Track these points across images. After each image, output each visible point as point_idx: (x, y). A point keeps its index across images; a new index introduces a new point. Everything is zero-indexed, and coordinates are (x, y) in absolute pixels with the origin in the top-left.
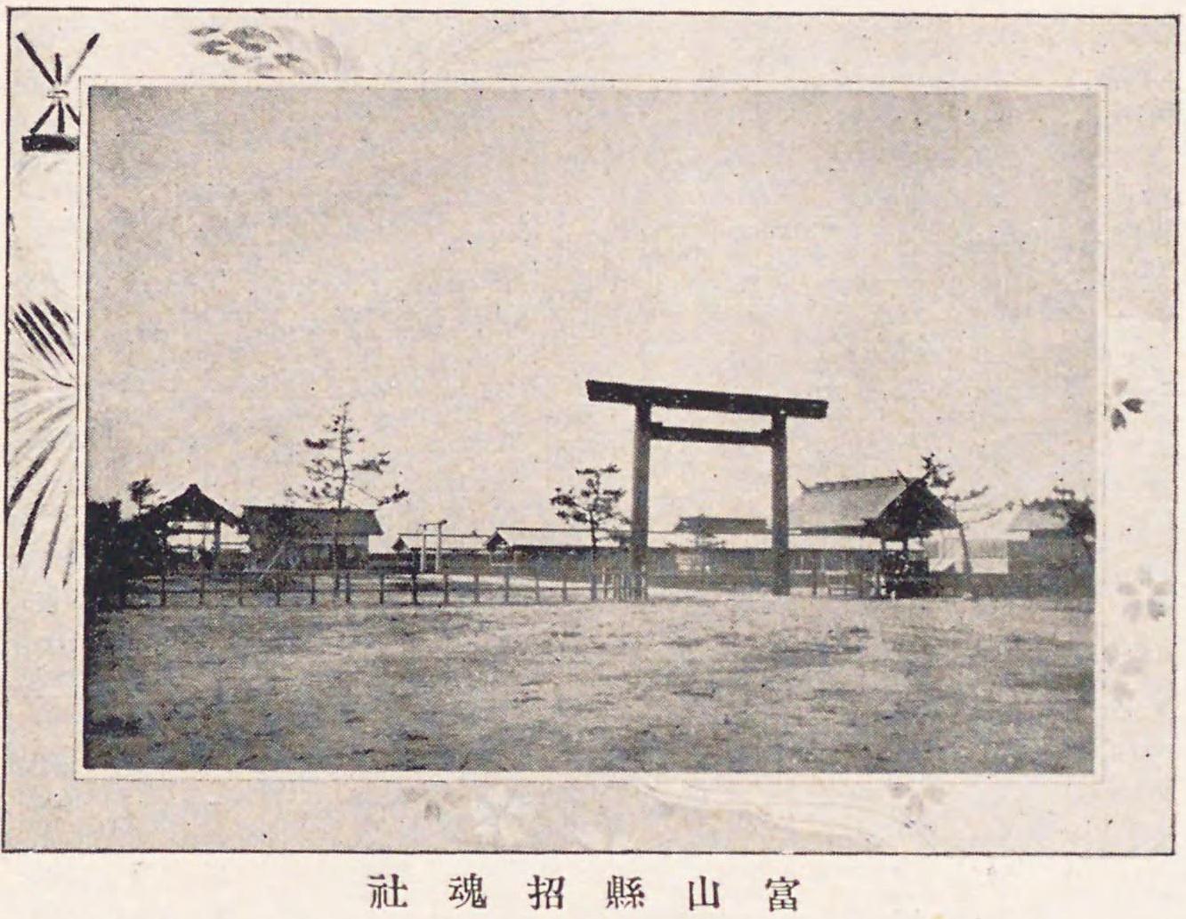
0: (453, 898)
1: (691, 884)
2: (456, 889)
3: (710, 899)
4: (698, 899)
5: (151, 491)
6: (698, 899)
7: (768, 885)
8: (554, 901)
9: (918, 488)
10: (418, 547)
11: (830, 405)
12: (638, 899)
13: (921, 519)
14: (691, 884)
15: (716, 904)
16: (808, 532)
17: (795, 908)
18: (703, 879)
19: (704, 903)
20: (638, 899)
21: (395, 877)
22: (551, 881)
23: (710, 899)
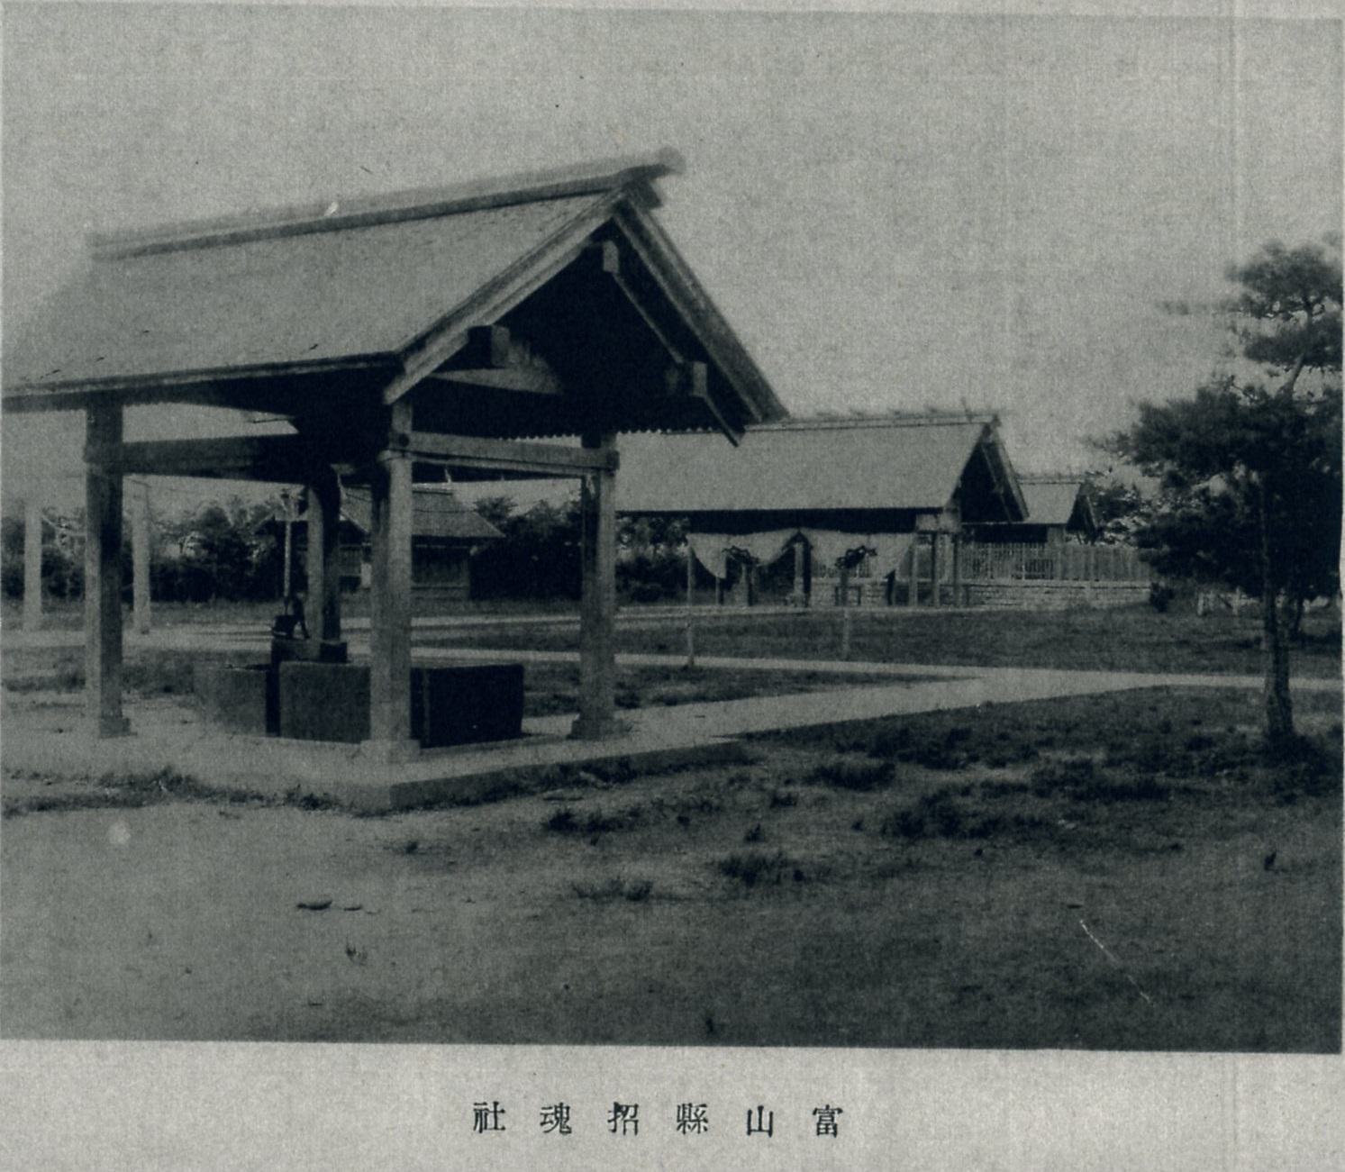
0: (543, 1124)
1: (750, 1113)
2: (546, 1115)
3: (765, 1127)
4: (755, 1126)
5: (272, 498)
6: (755, 1126)
7: (815, 1113)
8: (630, 1126)
9: (1153, 461)
10: (936, 506)
11: (1331, 1058)
12: (703, 1124)
13: (1320, 466)
14: (750, 1113)
15: (770, 1132)
16: (428, 643)
17: (835, 1134)
18: (761, 1109)
19: (760, 1129)
20: (703, 1124)
21: (496, 1104)
22: (628, 1107)
23: (765, 1127)
